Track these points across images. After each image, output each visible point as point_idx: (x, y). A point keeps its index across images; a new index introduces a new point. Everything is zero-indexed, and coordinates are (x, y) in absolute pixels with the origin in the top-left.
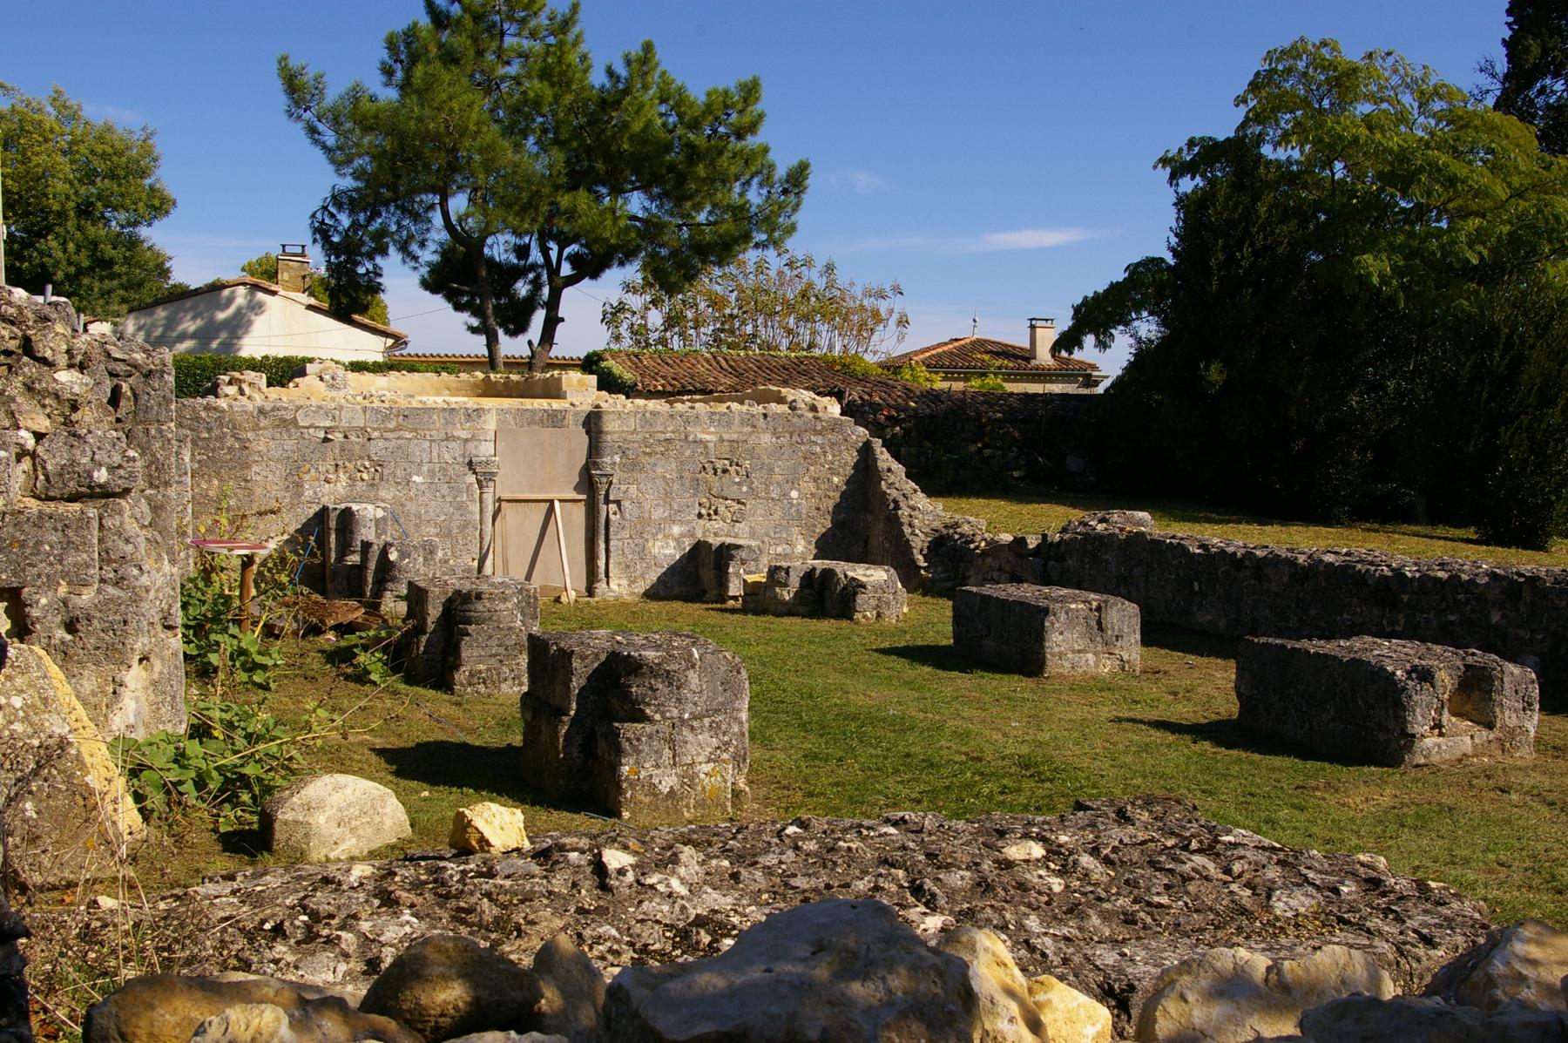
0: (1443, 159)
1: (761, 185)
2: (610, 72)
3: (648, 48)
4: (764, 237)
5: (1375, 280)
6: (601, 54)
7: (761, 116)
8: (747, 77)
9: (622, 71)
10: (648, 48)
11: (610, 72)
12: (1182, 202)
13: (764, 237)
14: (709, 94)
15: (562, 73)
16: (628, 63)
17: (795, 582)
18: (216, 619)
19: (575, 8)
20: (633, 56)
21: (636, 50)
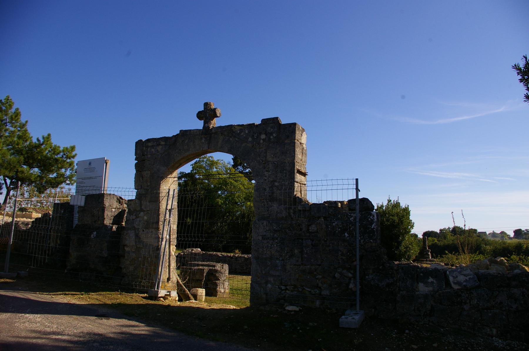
0: (233, 182)
1: (70, 170)
2: (38, 140)
3: (49, 135)
4: (69, 182)
5: (220, 204)
6: (35, 134)
7: (76, 155)
8: (72, 145)
9: (42, 141)
10: (49, 135)
11: (38, 140)
12: (179, 185)
13: (69, 182)
14: (441, 230)
15: (25, 138)
16: (43, 138)
17: (180, 252)
18: (400, 219)
19: (27, 122)
20: (45, 136)
21: (46, 135)
